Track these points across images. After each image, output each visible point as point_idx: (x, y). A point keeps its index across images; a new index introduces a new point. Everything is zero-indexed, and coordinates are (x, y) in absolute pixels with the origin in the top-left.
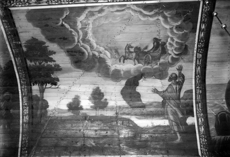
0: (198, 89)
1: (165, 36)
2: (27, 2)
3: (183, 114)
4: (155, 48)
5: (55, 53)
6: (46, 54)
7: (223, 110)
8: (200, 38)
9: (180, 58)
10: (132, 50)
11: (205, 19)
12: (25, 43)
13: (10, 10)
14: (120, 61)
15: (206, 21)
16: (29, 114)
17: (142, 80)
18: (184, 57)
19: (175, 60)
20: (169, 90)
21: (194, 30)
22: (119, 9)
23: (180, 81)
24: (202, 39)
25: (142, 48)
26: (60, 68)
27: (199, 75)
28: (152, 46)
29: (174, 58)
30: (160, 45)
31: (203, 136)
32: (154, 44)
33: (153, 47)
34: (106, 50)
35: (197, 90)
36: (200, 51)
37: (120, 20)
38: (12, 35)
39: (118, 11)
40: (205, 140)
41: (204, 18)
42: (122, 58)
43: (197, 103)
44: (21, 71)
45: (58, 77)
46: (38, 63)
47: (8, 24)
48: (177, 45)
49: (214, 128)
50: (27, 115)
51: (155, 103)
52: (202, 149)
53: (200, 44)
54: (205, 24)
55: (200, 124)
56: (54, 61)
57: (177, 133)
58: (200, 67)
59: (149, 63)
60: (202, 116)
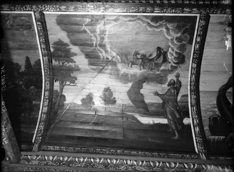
1: (166, 46)
2: (58, 8)
3: (180, 114)
4: (158, 56)
5: (76, 55)
7: (215, 114)
9: (179, 67)
10: (139, 57)
13: (43, 14)
14: (128, 66)
15: (201, 34)
16: (48, 106)
19: (174, 68)
20: (168, 93)
21: (191, 42)
23: (177, 87)
25: (147, 56)
27: (193, 82)
28: (156, 54)
29: (173, 66)
30: (162, 53)
31: (199, 135)
32: (157, 52)
36: (195, 61)
37: (131, 29)
39: (130, 21)
42: (131, 63)
43: (191, 106)
44: (46, 69)
46: (61, 64)
47: (41, 26)
49: (208, 128)
50: (46, 106)
52: (198, 146)
56: (75, 62)
58: (195, 75)
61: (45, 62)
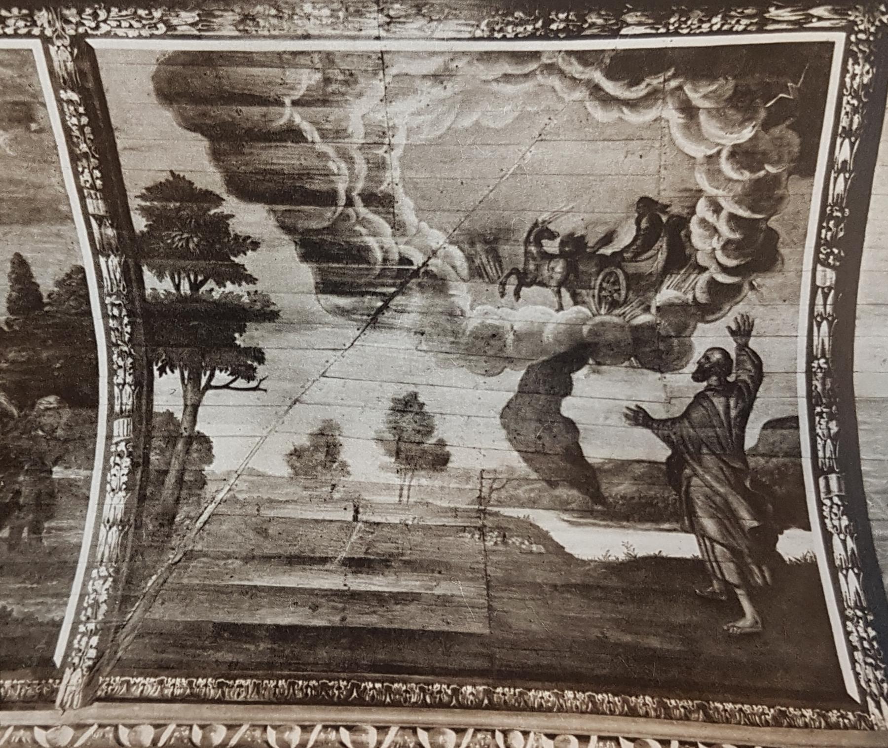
0: (822, 417)
3: (757, 511)
4: (644, 242)
5: (255, 245)
6: (220, 249)
8: (830, 201)
11: (851, 121)
12: (142, 197)
15: (855, 127)
17: (585, 370)
18: (759, 280)
19: (720, 296)
21: (804, 166)
22: (509, 69)
24: (835, 204)
26: (272, 308)
27: (823, 356)
30: (663, 225)
31: (859, 613)
32: (638, 223)
33: (635, 239)
34: (451, 243)
35: (817, 418)
36: (827, 255)
38: (94, 157)
40: (870, 630)
41: (847, 113)
42: (513, 280)
44: (116, 312)
45: (260, 346)
46: (185, 288)
47: (81, 110)
48: (733, 230)
50: (120, 489)
51: (637, 466)
53: (832, 223)
54: (853, 139)
55: (838, 563)
56: (252, 280)
57: (739, 591)
58: (830, 324)
59: (614, 305)
60: (846, 527)
61: (107, 283)
